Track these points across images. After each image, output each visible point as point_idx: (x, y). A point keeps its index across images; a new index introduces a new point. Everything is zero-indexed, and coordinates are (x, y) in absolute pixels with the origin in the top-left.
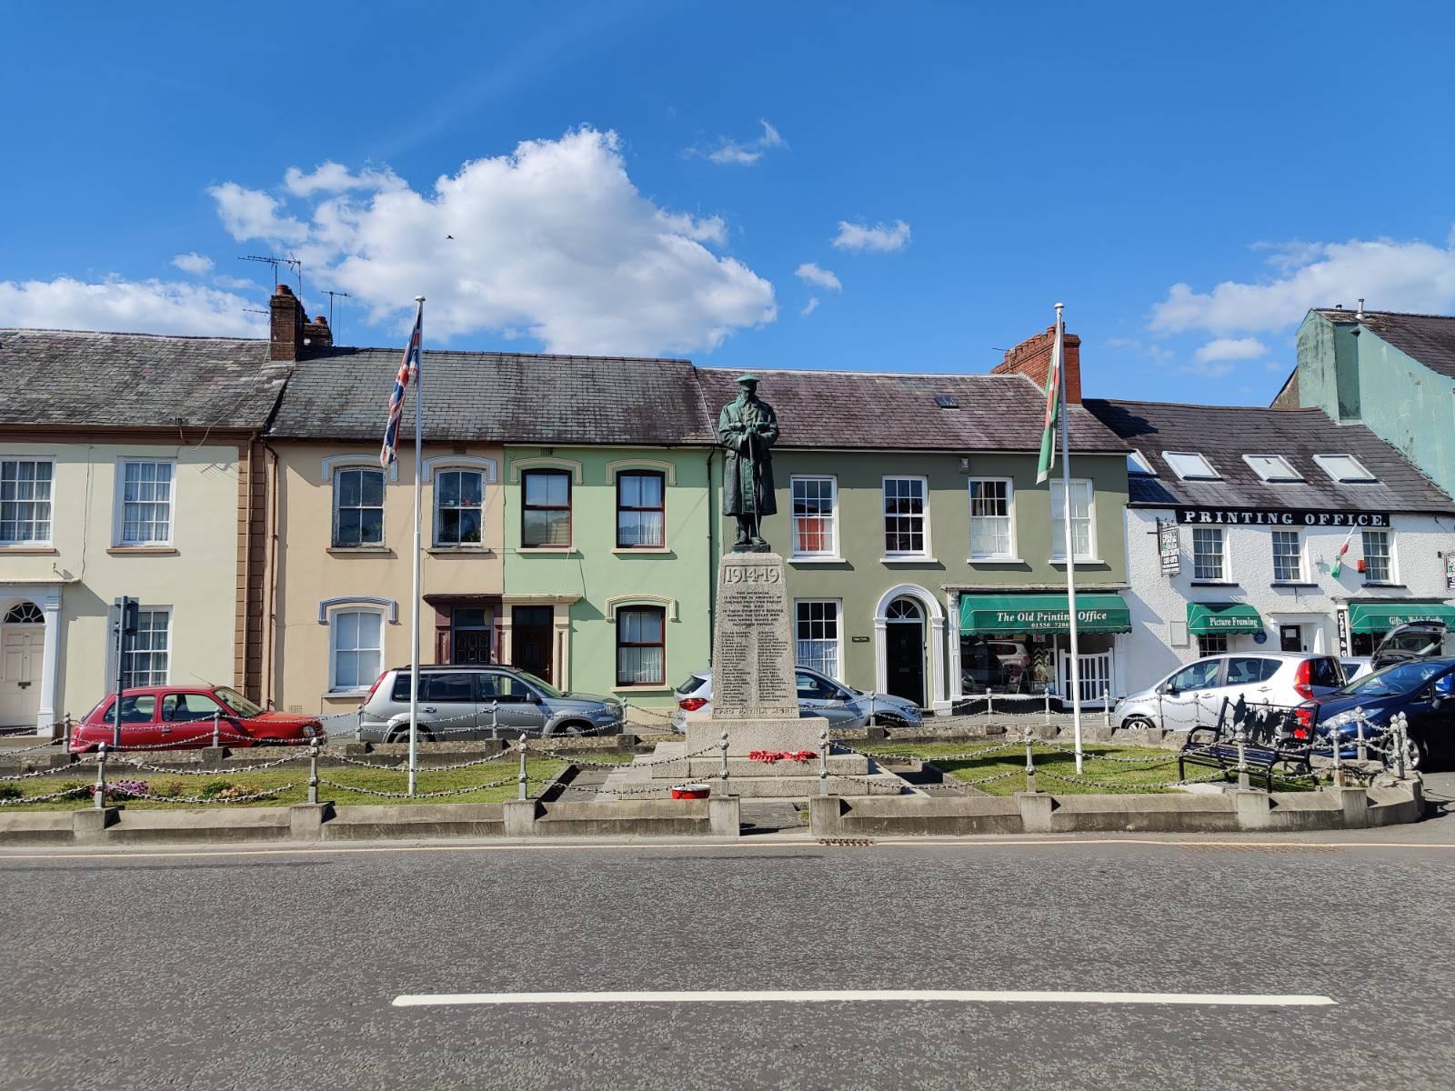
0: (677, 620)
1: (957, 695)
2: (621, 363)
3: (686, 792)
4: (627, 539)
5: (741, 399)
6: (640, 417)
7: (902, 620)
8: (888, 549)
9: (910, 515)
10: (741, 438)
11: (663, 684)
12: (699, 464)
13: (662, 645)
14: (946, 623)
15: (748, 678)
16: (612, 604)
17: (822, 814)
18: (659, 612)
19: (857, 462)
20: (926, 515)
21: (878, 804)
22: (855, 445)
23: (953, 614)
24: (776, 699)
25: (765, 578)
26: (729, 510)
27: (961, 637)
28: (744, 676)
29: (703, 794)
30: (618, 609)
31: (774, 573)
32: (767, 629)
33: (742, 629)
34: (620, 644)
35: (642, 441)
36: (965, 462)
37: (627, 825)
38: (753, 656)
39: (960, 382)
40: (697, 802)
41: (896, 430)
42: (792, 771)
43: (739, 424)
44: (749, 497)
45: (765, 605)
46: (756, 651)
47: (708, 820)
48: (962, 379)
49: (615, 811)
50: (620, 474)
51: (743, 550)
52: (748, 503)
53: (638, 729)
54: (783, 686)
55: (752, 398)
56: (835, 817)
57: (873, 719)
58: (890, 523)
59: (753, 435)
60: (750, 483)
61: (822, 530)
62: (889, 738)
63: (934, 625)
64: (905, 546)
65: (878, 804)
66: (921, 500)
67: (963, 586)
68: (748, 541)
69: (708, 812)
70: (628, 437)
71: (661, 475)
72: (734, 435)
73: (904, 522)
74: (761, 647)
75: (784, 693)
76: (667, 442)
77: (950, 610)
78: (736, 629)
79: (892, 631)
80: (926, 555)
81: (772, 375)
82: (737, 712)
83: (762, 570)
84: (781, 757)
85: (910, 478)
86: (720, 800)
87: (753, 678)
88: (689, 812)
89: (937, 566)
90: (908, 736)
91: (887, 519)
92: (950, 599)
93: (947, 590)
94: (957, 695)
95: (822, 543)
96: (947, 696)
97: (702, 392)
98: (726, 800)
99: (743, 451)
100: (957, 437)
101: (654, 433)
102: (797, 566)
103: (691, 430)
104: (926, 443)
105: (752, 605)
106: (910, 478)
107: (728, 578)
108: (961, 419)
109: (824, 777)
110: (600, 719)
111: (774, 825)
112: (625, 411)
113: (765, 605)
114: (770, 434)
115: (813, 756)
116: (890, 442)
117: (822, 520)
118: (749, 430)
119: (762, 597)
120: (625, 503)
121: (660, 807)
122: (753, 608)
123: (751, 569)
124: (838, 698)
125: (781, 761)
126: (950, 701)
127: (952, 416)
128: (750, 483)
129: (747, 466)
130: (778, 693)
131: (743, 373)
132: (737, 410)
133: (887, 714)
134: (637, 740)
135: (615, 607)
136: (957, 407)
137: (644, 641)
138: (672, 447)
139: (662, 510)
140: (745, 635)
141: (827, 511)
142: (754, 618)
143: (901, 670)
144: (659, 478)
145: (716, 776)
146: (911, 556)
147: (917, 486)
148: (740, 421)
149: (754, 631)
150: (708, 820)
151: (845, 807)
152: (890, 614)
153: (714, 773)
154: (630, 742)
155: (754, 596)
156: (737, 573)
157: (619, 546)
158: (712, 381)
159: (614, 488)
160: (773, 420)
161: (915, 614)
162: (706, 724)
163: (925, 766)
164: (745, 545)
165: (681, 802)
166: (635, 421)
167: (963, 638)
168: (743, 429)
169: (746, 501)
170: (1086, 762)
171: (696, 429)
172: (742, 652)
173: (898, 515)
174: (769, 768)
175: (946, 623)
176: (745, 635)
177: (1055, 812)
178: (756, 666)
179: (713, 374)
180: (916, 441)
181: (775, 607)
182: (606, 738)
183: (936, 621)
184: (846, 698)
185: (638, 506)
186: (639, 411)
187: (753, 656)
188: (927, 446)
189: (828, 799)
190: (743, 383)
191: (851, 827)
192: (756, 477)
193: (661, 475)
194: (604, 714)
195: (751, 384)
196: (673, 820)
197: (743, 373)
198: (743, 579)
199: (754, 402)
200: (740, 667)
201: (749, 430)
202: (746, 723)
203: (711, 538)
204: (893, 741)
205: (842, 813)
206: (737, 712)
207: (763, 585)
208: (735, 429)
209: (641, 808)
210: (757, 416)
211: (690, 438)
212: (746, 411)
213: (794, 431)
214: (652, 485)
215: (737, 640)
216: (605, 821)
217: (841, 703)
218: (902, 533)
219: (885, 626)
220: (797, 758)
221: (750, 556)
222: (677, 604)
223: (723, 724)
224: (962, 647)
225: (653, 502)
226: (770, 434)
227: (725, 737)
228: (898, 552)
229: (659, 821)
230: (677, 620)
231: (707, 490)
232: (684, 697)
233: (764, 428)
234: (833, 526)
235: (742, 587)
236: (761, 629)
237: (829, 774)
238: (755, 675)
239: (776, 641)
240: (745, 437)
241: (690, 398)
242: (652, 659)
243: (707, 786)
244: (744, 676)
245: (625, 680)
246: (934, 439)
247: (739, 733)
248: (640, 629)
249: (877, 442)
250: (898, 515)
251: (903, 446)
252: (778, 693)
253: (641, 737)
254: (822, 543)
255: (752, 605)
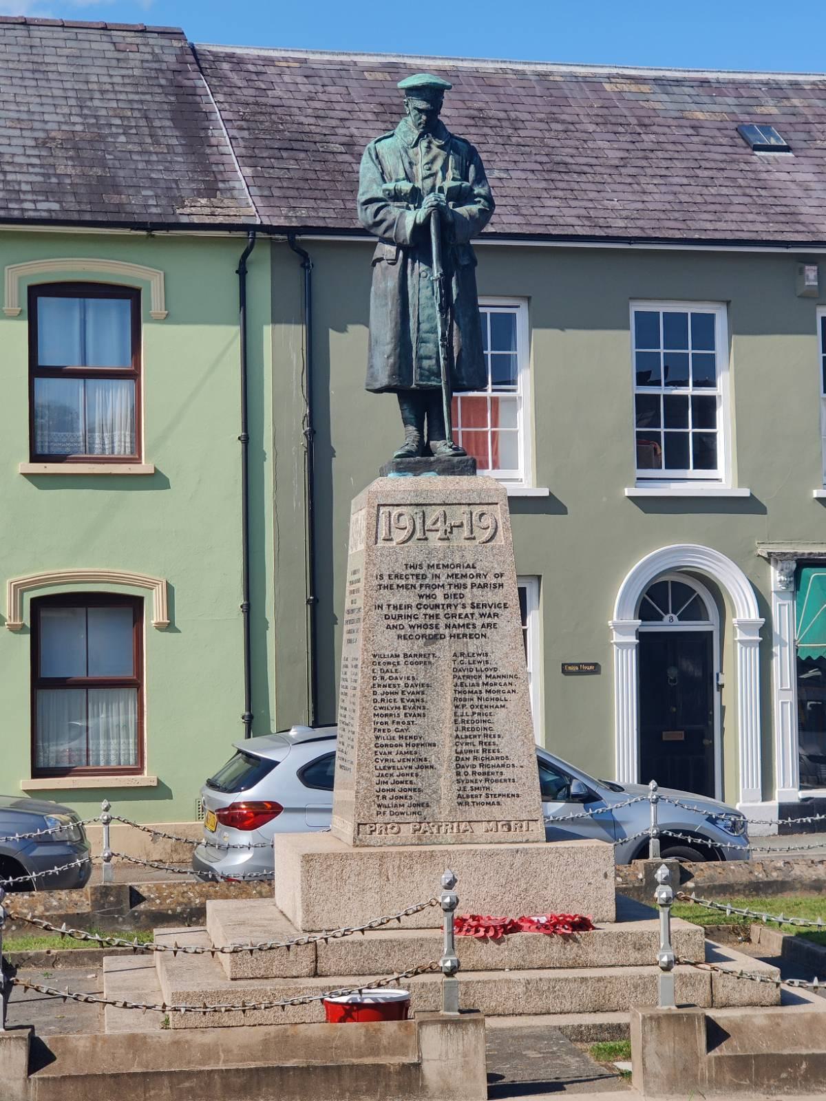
0: (169, 627)
1: (788, 790)
2: (21, 32)
3: (359, 1006)
4: (52, 441)
5: (407, 129)
6: (77, 159)
7: (671, 624)
8: (641, 465)
9: (689, 391)
10: (411, 218)
11: (138, 771)
12: (218, 270)
13: (135, 684)
14: (766, 631)
15: (430, 755)
16: (20, 589)
17: (667, 1049)
18: (133, 606)
19: (588, 270)
20: (724, 389)
21: (785, 1025)
22: (570, 231)
23: (783, 612)
24: (494, 800)
25: (466, 532)
26: (383, 380)
27: (798, 660)
28: (424, 753)
29: (396, 1010)
30: (33, 601)
31: (487, 521)
32: (473, 646)
33: (418, 646)
34: (40, 683)
35: (87, 217)
36: (811, 272)
37: (237, 1081)
38: (442, 706)
39: (790, 93)
40: (390, 1027)
41: (658, 198)
42: (538, 958)
43: (406, 186)
44: (430, 349)
45: (467, 592)
46: (449, 695)
47: (417, 1066)
48: (795, 85)
49: (209, 1052)
50: (36, 292)
51: (416, 470)
52: (426, 363)
53: (134, 872)
54: (507, 773)
55: (431, 127)
56: (694, 1053)
57: (654, 845)
58: (645, 406)
59: (439, 209)
60: (431, 318)
61: (495, 424)
62: (690, 884)
63: (740, 636)
64: (676, 461)
65: (785, 1025)
66: (712, 358)
67: (805, 550)
68: (424, 450)
69: (419, 1050)
70: (56, 206)
71: (132, 295)
72: (394, 210)
73: (676, 404)
74: (460, 688)
75: (511, 788)
76: (147, 219)
77: (775, 604)
78: (403, 647)
79: (652, 653)
80: (723, 479)
81: (372, 69)
82: (407, 830)
83: (459, 515)
84: (514, 927)
85: (689, 308)
86: (445, 1022)
87: (444, 754)
88: (374, 1051)
89: (748, 505)
90: (731, 879)
91: (639, 398)
92: (775, 577)
93: (770, 558)
94: (788, 790)
95: (495, 452)
96: (767, 793)
97: (213, 103)
98: (456, 1023)
99: (416, 248)
100: (792, 216)
101: (115, 199)
102: (648, 504)
103: (200, 194)
104: (725, 228)
105: (439, 593)
106: (689, 308)
107: (383, 533)
108: (800, 177)
109: (667, 969)
110: (40, 851)
111: (545, 1075)
112: (42, 144)
113: (467, 592)
114: (474, 208)
115: (583, 924)
116: (647, 227)
117: (495, 401)
118: (429, 200)
119: (461, 575)
120: (48, 358)
121: (203, 1045)
122: (440, 600)
123: (434, 513)
124: (570, 798)
125: (515, 937)
126: (774, 803)
127: (777, 168)
128: (431, 318)
129: (425, 281)
130: (497, 788)
131: (412, 71)
132: (394, 159)
133: (686, 833)
134: (136, 897)
135: (28, 597)
136: (787, 149)
137: (95, 674)
138: (154, 230)
139: (132, 375)
140: (425, 660)
141: (506, 378)
142: (442, 622)
143: (667, 736)
144: (127, 303)
145: (432, 970)
146: (691, 483)
147: (705, 325)
148: (408, 178)
149: (445, 651)
150: (417, 1066)
151: (716, 1035)
152: (645, 611)
153: (428, 961)
154: (119, 902)
155: (443, 573)
156: (405, 522)
157: (35, 458)
158: (235, 79)
159: (24, 325)
160: (481, 178)
161: (696, 611)
162: (343, 857)
163: (786, 942)
164: (418, 459)
165: (353, 1030)
166: (65, 168)
167: (803, 665)
168: (415, 197)
169: (420, 358)
170: (285, 948)
171: (211, 190)
172: (417, 704)
173: (662, 391)
174: (488, 952)
175: (766, 631)
176: (425, 660)
177: (713, 1054)
178: (448, 729)
179: (237, 62)
180: (703, 225)
181: (490, 597)
182: (63, 894)
183: (744, 626)
184: (589, 798)
185: (76, 365)
186: (73, 145)
187: (442, 706)
188: (729, 236)
189: (678, 1017)
190: (413, 91)
191: (729, 1077)
192: (446, 305)
193: (132, 295)
194: (46, 841)
195: (432, 94)
196: (339, 1068)
197: (412, 71)
198: (418, 535)
199: (436, 136)
200: (414, 730)
201: (429, 200)
202: (432, 855)
203: (246, 440)
204: (699, 890)
205: (711, 1046)
206: (407, 830)
207: (464, 549)
208: (396, 196)
209: (266, 1042)
210: (444, 168)
211: (197, 210)
212: (420, 155)
213: (519, 201)
214: (109, 319)
215: (405, 670)
216: (189, 1075)
217: (578, 810)
218: (671, 429)
219: (634, 640)
220: (551, 927)
221: (432, 483)
222: (170, 590)
223: (382, 857)
224: (801, 684)
225: (111, 356)
226: (474, 208)
227: (450, 885)
228: (664, 473)
229: (306, 1071)
230: (169, 627)
231: (236, 330)
232: (229, 799)
233: (460, 196)
234: (520, 415)
235: (413, 551)
236: (458, 646)
237: (677, 961)
238: (446, 750)
239: (493, 675)
240: (420, 215)
241: (189, 118)
242: (110, 715)
243: (403, 993)
244: (424, 753)
245: (52, 764)
246: (743, 222)
247: (417, 878)
248: (88, 647)
249: (618, 226)
250: (662, 391)
251: (678, 235)
252: (497, 788)
253: (143, 891)
254: (495, 452)
255: (439, 593)
